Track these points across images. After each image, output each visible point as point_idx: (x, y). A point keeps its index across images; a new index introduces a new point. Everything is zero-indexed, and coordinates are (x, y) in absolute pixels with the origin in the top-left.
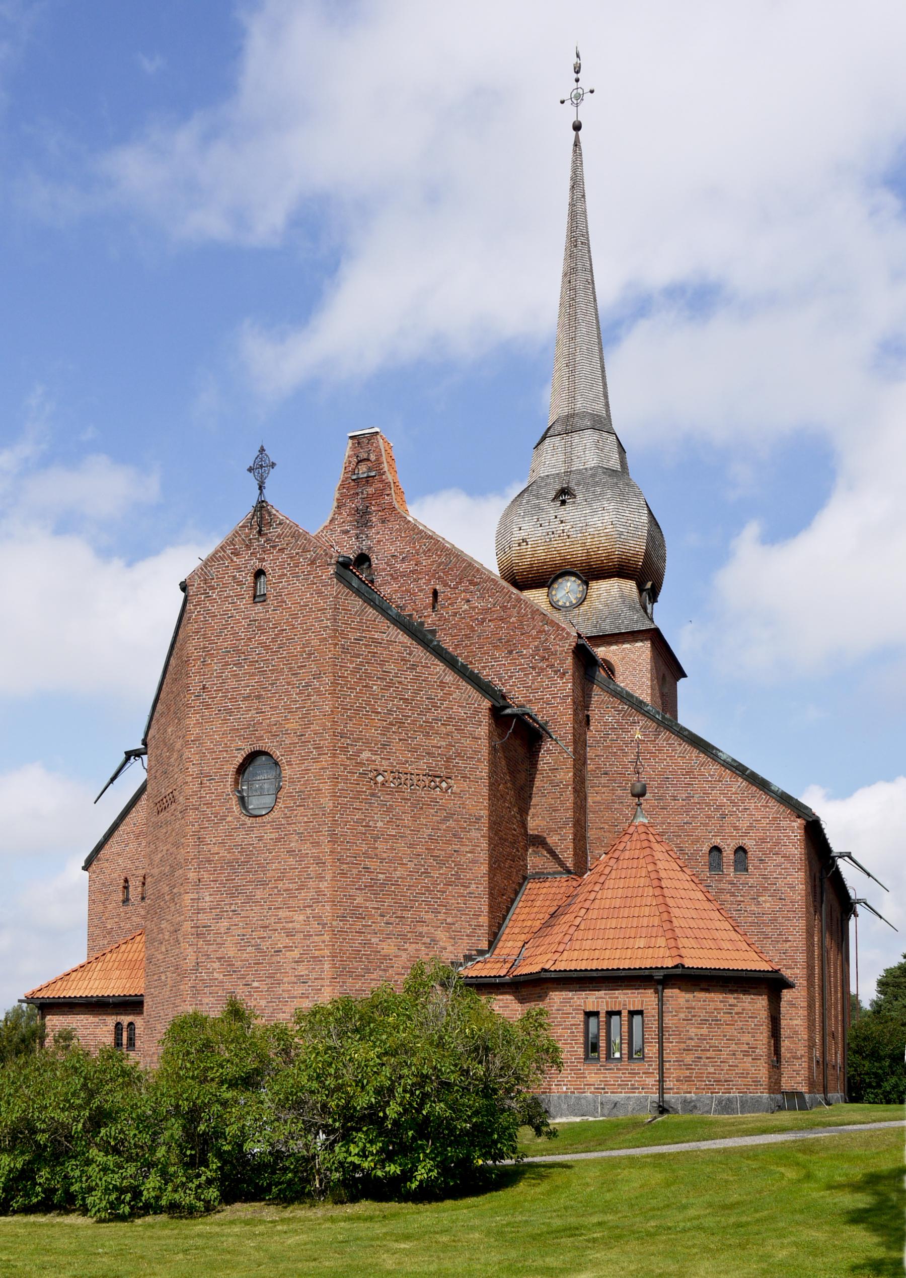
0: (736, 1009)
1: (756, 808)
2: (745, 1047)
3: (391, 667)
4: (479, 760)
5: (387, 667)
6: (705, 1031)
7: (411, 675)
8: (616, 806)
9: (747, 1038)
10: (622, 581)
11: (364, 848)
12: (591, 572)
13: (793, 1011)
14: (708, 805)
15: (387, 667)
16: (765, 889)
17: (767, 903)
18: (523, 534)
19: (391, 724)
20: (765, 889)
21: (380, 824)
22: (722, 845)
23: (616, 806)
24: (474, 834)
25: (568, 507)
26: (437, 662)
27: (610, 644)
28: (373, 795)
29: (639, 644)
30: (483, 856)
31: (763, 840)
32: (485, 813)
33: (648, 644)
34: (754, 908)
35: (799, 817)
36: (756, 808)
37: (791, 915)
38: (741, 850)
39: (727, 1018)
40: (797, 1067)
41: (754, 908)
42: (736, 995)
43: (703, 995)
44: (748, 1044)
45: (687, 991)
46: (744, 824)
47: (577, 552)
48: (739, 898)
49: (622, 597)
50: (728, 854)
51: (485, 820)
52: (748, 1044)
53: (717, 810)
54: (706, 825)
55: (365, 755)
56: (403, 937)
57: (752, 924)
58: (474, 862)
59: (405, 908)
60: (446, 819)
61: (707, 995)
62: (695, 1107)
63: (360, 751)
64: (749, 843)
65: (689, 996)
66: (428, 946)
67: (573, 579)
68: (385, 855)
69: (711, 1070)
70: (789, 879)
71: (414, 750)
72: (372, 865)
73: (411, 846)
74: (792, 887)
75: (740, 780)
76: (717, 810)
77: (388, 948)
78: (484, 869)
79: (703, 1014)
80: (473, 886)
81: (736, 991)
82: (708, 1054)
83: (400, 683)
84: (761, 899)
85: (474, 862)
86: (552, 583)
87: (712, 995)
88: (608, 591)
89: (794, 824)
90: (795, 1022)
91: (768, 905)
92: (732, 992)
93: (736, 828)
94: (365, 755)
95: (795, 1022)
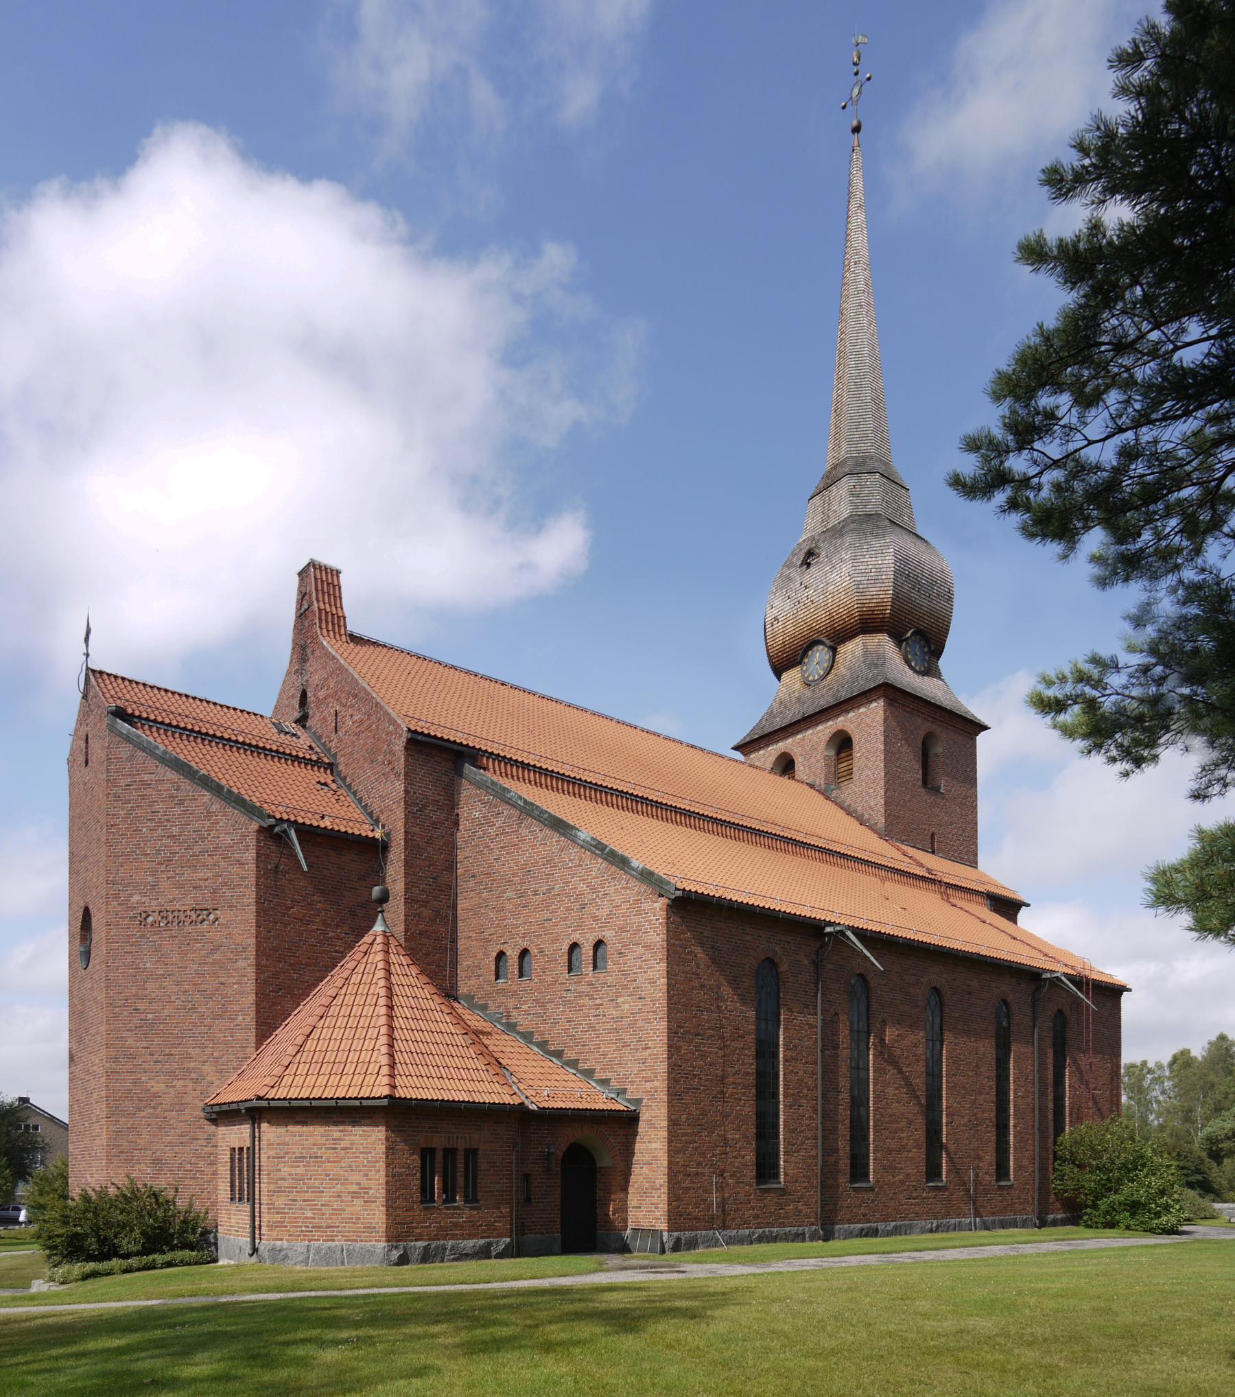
0: (343, 1144)
1: (616, 891)
2: (354, 1188)
3: (160, 807)
4: (246, 887)
5: (156, 807)
6: (300, 1170)
7: (178, 810)
8: (483, 910)
9: (355, 1178)
10: (868, 637)
11: (134, 990)
12: (838, 636)
13: (652, 1132)
14: (569, 896)
15: (156, 807)
16: (625, 987)
17: (627, 1003)
18: (775, 611)
19: (159, 864)
20: (625, 987)
21: (148, 965)
22: (581, 940)
23: (483, 910)
24: (241, 964)
25: (813, 569)
26: (204, 792)
27: (847, 711)
28: (142, 937)
29: (874, 705)
30: (250, 985)
31: (623, 930)
32: (252, 941)
33: (881, 702)
34: (612, 1012)
35: (661, 896)
36: (616, 891)
37: (651, 1016)
38: (599, 944)
39: (330, 1154)
40: (655, 1200)
41: (612, 1012)
42: (342, 1128)
43: (298, 1128)
44: (358, 1184)
45: (278, 1124)
46: (603, 913)
47: (820, 617)
48: (598, 1001)
49: (865, 655)
50: (587, 951)
51: (252, 949)
52: (358, 1184)
53: (576, 900)
54: (565, 919)
55: (135, 898)
56: (172, 1074)
57: (610, 1031)
58: (241, 992)
59: (173, 1046)
60: (213, 951)
61: (305, 1128)
62: (286, 1256)
63: (131, 895)
64: (608, 935)
65: (281, 1130)
66: (195, 1081)
67: (821, 647)
68: (153, 995)
69: (309, 1214)
70: (650, 974)
71: (180, 887)
72: (141, 1005)
73: (178, 983)
74: (652, 982)
75: (600, 860)
76: (576, 900)
77: (157, 1087)
78: (251, 998)
79: (297, 1150)
80: (240, 1018)
81: (343, 1123)
82: (307, 1196)
83: (168, 820)
84: (620, 1000)
85: (241, 992)
86: (802, 658)
87: (311, 1128)
88: (853, 652)
89: (656, 905)
90: (654, 1146)
91: (627, 1006)
92: (336, 1123)
93: (596, 919)
94: (135, 898)
95: (654, 1146)
